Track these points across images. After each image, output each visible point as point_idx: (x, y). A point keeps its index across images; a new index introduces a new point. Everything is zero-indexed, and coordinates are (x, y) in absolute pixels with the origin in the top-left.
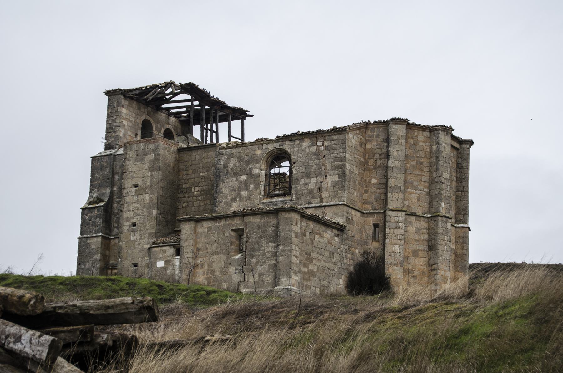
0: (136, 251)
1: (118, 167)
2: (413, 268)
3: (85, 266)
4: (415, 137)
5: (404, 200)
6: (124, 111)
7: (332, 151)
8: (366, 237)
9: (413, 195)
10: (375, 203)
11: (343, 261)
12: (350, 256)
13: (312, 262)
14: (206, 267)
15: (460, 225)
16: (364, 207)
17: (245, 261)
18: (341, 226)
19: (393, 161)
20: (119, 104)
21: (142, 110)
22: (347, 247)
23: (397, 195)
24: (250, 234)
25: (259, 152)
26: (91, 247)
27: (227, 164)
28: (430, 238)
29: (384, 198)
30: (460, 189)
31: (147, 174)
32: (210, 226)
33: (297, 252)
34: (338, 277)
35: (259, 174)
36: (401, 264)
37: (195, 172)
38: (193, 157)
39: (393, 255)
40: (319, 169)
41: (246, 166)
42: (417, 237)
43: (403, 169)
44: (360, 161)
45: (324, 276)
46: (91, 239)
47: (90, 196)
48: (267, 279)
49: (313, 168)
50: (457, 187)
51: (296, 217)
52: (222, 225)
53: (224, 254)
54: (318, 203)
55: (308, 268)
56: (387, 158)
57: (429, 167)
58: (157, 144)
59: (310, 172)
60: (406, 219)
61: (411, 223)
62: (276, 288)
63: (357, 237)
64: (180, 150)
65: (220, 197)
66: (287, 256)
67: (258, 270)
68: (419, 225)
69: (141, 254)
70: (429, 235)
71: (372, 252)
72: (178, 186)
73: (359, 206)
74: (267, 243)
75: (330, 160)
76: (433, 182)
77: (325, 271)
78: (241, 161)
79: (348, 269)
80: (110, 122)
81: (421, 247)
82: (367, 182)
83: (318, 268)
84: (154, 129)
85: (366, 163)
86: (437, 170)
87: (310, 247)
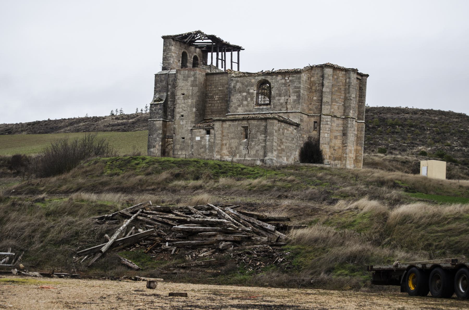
0: (183, 131)
1: (170, 81)
5: (331, 109)
6: (173, 48)
7: (293, 83)
9: (336, 106)
10: (315, 110)
12: (301, 139)
13: (283, 144)
14: (228, 145)
15: (360, 121)
20: (170, 44)
21: (182, 46)
22: (300, 135)
23: (327, 107)
25: (253, 81)
35: (253, 93)
36: (328, 143)
37: (216, 87)
38: (215, 79)
42: (337, 128)
43: (331, 93)
47: (155, 97)
50: (359, 100)
51: (276, 122)
53: (237, 139)
58: (195, 71)
60: (331, 119)
61: (334, 121)
63: (305, 129)
64: (207, 74)
65: (231, 104)
69: (187, 132)
72: (206, 94)
73: (306, 112)
74: (260, 135)
75: (292, 88)
76: (346, 99)
79: (300, 146)
80: (165, 54)
81: (339, 134)
84: (188, 57)
85: (311, 88)
86: (349, 93)
87: (282, 136)
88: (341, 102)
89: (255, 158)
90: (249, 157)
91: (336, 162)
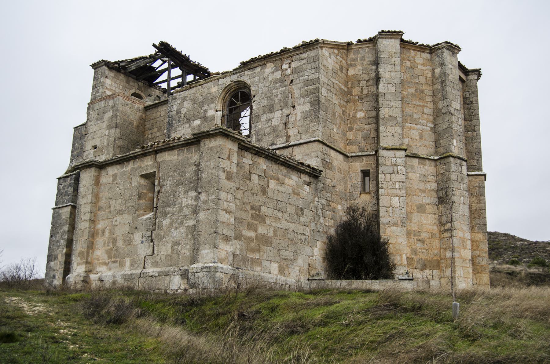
2: (419, 228)
3: (56, 238)
4: (412, 59)
6: (108, 82)
7: (301, 74)
8: (352, 188)
9: (414, 131)
10: (363, 143)
11: (318, 221)
12: (329, 213)
13: (264, 222)
14: (107, 234)
16: (348, 149)
17: (156, 223)
18: (313, 169)
19: (385, 85)
21: (131, 84)
22: (324, 201)
23: (392, 130)
24: (164, 180)
26: (62, 218)
27: (180, 109)
28: (441, 187)
29: (375, 136)
30: (470, 129)
31: (105, 133)
32: (116, 173)
33: (231, 204)
34: (311, 245)
35: (214, 115)
37: (160, 129)
39: (391, 211)
40: (285, 99)
41: (200, 109)
42: (422, 186)
44: (341, 89)
45: (287, 244)
46: (63, 209)
48: (183, 251)
49: (278, 98)
50: (465, 126)
52: (130, 171)
53: (129, 213)
54: (284, 143)
55: (256, 230)
56: (376, 85)
57: (432, 96)
59: (273, 105)
60: (406, 163)
61: (412, 167)
62: (193, 266)
63: (340, 188)
66: (211, 210)
67: (171, 236)
68: (424, 170)
70: (437, 184)
71: (361, 208)
73: (341, 146)
74: (186, 192)
75: (299, 86)
76: (437, 114)
77: (289, 236)
78: (195, 103)
79: (326, 232)
80: (94, 93)
81: (430, 199)
82: (351, 117)
83: (275, 232)
85: (350, 93)
86: (444, 98)
88: (428, 121)
89: (167, 269)
90: (155, 264)
91: (428, 272)
